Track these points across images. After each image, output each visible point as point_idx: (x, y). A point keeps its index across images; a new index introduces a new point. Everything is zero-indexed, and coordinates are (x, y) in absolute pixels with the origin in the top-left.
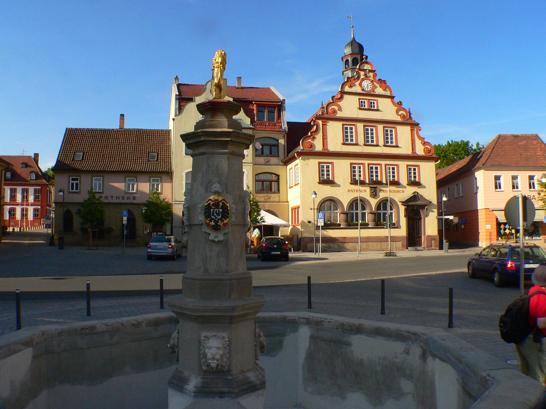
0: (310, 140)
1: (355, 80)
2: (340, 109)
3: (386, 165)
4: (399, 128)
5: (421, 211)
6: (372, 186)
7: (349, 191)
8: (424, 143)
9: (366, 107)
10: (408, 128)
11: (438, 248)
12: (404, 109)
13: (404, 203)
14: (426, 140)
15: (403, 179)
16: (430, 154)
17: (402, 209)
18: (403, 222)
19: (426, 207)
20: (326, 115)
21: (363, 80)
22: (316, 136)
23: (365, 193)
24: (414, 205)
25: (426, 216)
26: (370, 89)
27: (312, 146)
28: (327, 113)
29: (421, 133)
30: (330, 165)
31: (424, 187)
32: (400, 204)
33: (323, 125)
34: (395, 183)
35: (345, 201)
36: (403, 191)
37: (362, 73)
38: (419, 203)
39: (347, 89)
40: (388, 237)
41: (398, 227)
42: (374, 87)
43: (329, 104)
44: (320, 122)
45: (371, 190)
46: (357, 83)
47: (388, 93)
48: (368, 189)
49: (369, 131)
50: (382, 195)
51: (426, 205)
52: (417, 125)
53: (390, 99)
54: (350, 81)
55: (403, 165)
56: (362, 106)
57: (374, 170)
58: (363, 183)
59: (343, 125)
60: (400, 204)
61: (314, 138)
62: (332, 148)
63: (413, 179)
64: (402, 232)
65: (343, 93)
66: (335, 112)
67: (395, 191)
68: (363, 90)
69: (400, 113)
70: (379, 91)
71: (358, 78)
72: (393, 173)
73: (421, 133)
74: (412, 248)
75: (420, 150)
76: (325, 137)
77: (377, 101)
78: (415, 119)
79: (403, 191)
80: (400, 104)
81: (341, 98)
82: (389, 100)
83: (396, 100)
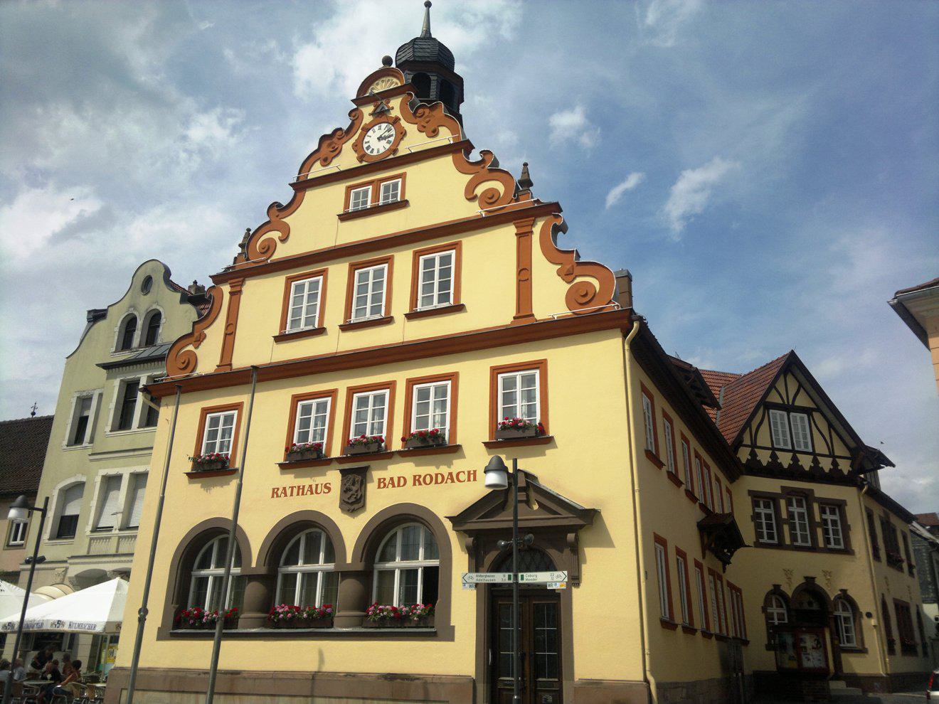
0: (190, 348)
6: (347, 466)
7: (275, 492)
23: (322, 495)
34: (431, 445)
35: (257, 529)
38: (533, 514)
43: (261, 229)
46: (347, 147)
50: (379, 500)
55: (474, 374)
67: (435, 479)
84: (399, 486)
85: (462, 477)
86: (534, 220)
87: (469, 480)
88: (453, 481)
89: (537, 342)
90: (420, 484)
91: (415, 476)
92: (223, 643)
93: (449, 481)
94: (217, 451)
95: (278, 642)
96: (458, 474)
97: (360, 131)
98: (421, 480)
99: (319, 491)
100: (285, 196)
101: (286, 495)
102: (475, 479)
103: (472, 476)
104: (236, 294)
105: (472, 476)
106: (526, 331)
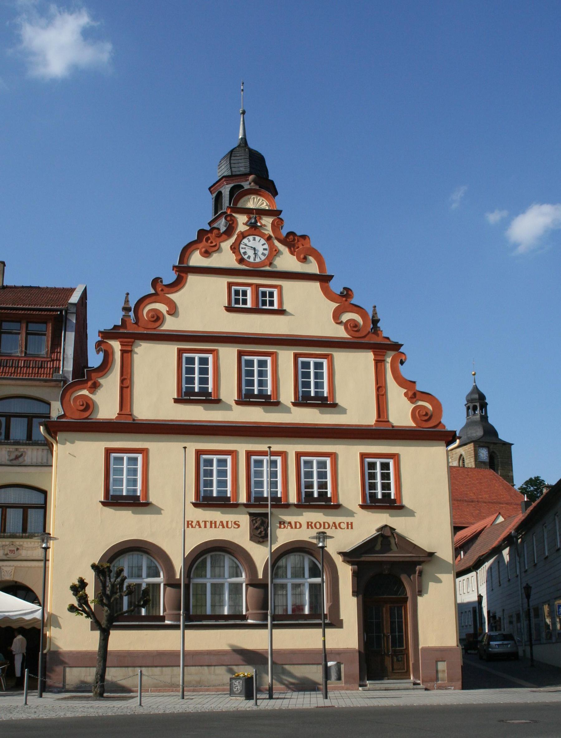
0: (85, 392)
1: (219, 236)
2: (173, 310)
3: (299, 455)
4: (341, 358)
5: (404, 578)
8: (414, 395)
9: (249, 305)
10: (368, 357)
11: (459, 683)
12: (357, 309)
13: (349, 556)
14: (419, 387)
15: (350, 491)
16: (431, 423)
17: (346, 573)
18: (349, 607)
19: (418, 568)
20: (137, 329)
21: (243, 235)
22: (101, 381)
23: (236, 529)
24: (381, 563)
25: (420, 593)
26: (261, 258)
27: (89, 406)
28: (136, 323)
29: (405, 371)
30: (229, 458)
31: (411, 513)
32: (338, 560)
33: (123, 352)
34: (326, 503)
36: (350, 526)
37: (242, 219)
38: (394, 555)
39: (196, 259)
40: (179, 651)
41: (337, 623)
42: (274, 253)
44: (116, 345)
45: (252, 522)
46: (226, 246)
47: (312, 268)
48: (244, 520)
49: (197, 366)
51: (420, 563)
52: (396, 347)
53: (317, 285)
54: (206, 239)
55: (349, 455)
56: (264, 303)
57: (378, 471)
58: (223, 503)
59: (296, 356)
60: (338, 560)
61: (95, 387)
62: (143, 411)
63: (215, 489)
64: (347, 637)
65: (184, 270)
66: (158, 318)
68: (241, 261)
69: (346, 317)
70: (287, 261)
71: (229, 231)
72: (386, 476)
73: (405, 371)
74: (378, 684)
75: (401, 413)
76: (126, 384)
77: (280, 288)
78: (389, 330)
79: (350, 526)
80: (347, 294)
81: (178, 284)
82: (316, 286)
83: (336, 286)
84: (296, 528)
85: (342, 525)
86: (133, 342)
87: (348, 528)
88: (336, 528)
89: (187, 436)
90: (312, 528)
91: (308, 523)
92: (326, 630)
93: (334, 528)
94: (215, 489)
95: (142, 631)
96: (339, 524)
97: (235, 237)
98: (313, 525)
99: (230, 525)
100: (170, 277)
101: (200, 527)
102: (352, 528)
103: (350, 526)
104: (127, 353)
105: (350, 526)
106: (384, 432)
